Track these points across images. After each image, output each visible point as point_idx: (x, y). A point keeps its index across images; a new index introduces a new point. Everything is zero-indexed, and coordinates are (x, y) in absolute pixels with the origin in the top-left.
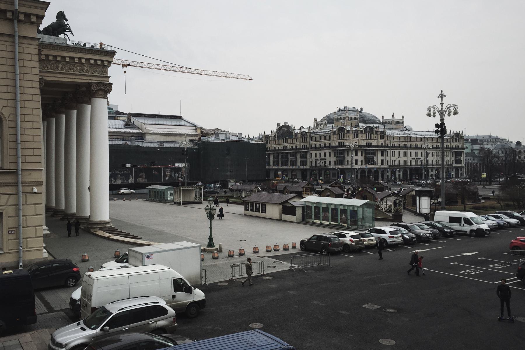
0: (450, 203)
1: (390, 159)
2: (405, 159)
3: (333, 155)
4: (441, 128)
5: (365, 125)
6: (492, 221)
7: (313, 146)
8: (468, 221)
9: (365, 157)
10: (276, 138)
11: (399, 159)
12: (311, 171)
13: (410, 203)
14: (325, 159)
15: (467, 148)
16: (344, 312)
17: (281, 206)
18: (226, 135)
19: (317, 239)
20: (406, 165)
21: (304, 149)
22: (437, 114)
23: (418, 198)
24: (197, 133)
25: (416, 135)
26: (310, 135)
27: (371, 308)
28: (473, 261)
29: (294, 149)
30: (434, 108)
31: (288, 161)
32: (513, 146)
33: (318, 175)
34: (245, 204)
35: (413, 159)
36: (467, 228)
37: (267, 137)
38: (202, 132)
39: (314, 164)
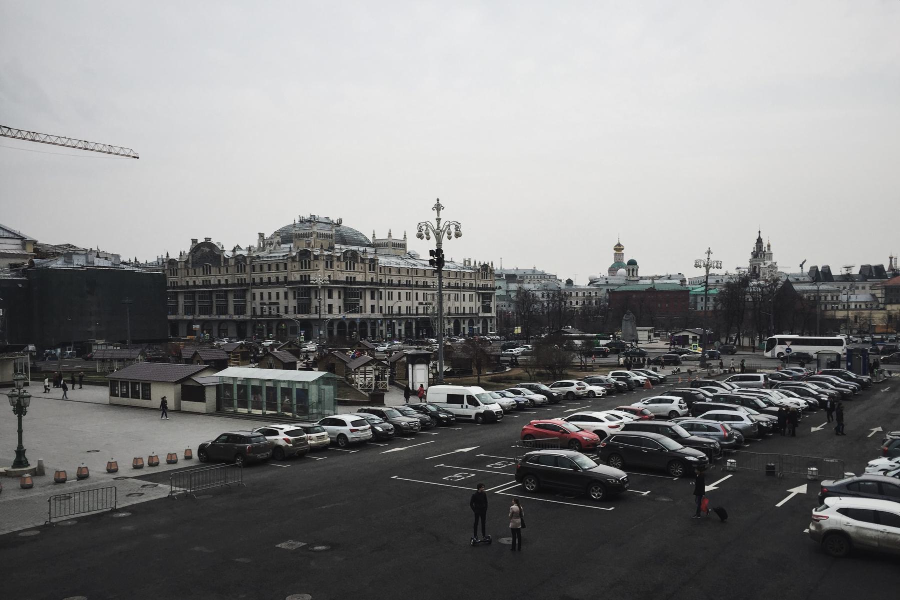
0: (460, 371)
2: (409, 304)
3: (291, 295)
4: (438, 257)
5: (344, 248)
6: (509, 400)
7: (257, 280)
8: (472, 401)
9: (345, 300)
10: (190, 266)
11: (399, 304)
12: (255, 323)
13: (396, 373)
14: (278, 304)
15: (500, 288)
16: (241, 560)
17: (179, 386)
18: (87, 258)
19: (226, 441)
20: (410, 314)
21: (241, 285)
22: (431, 234)
23: (410, 366)
24: (25, 252)
26: (251, 262)
27: (290, 548)
28: (469, 461)
29: (223, 286)
30: (427, 225)
31: (212, 306)
32: (563, 285)
33: (265, 331)
34: (113, 385)
35: (420, 304)
36: (471, 411)
37: (172, 262)
38: (36, 250)
39: (258, 312)
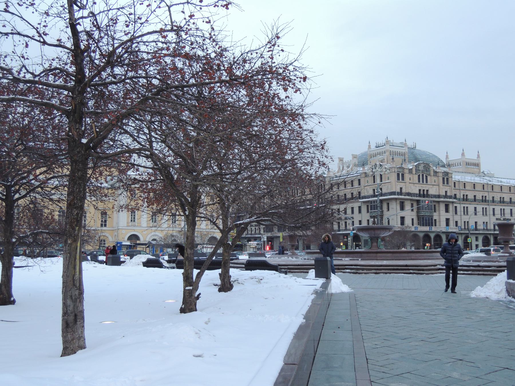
1: (460, 218)
2: (486, 219)
9: (418, 212)
14: (353, 218)
20: (487, 230)
25: (501, 182)
